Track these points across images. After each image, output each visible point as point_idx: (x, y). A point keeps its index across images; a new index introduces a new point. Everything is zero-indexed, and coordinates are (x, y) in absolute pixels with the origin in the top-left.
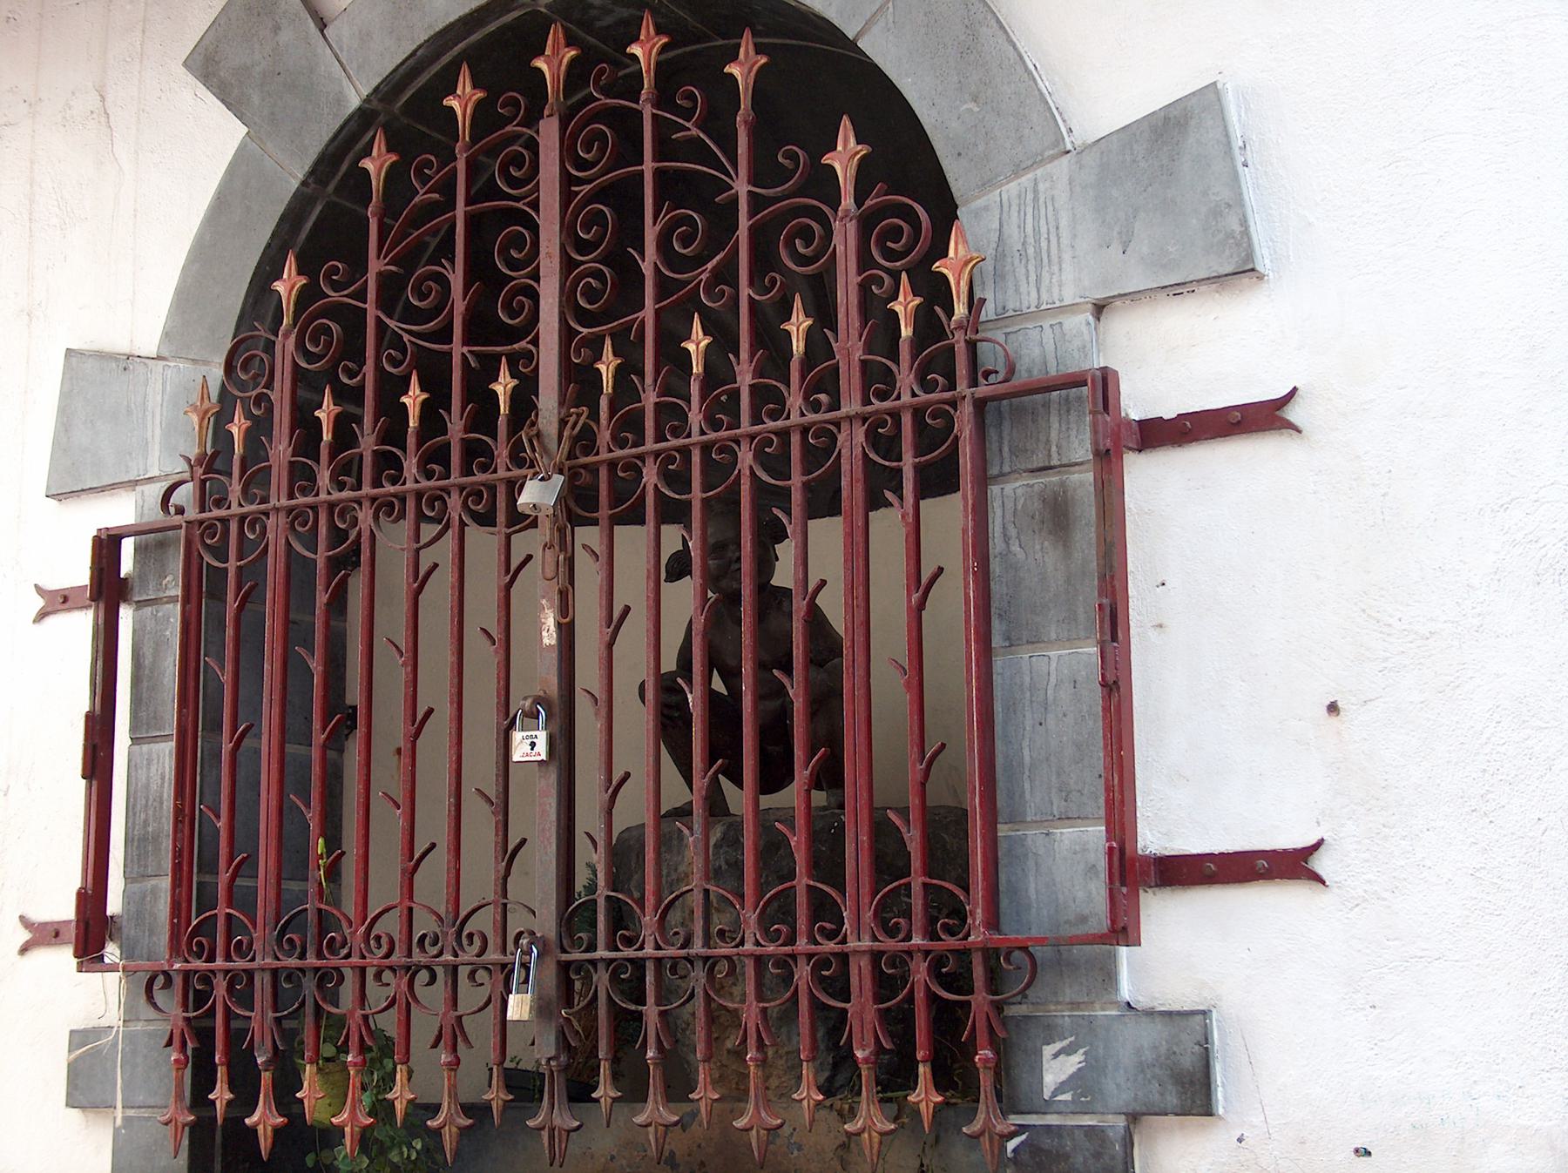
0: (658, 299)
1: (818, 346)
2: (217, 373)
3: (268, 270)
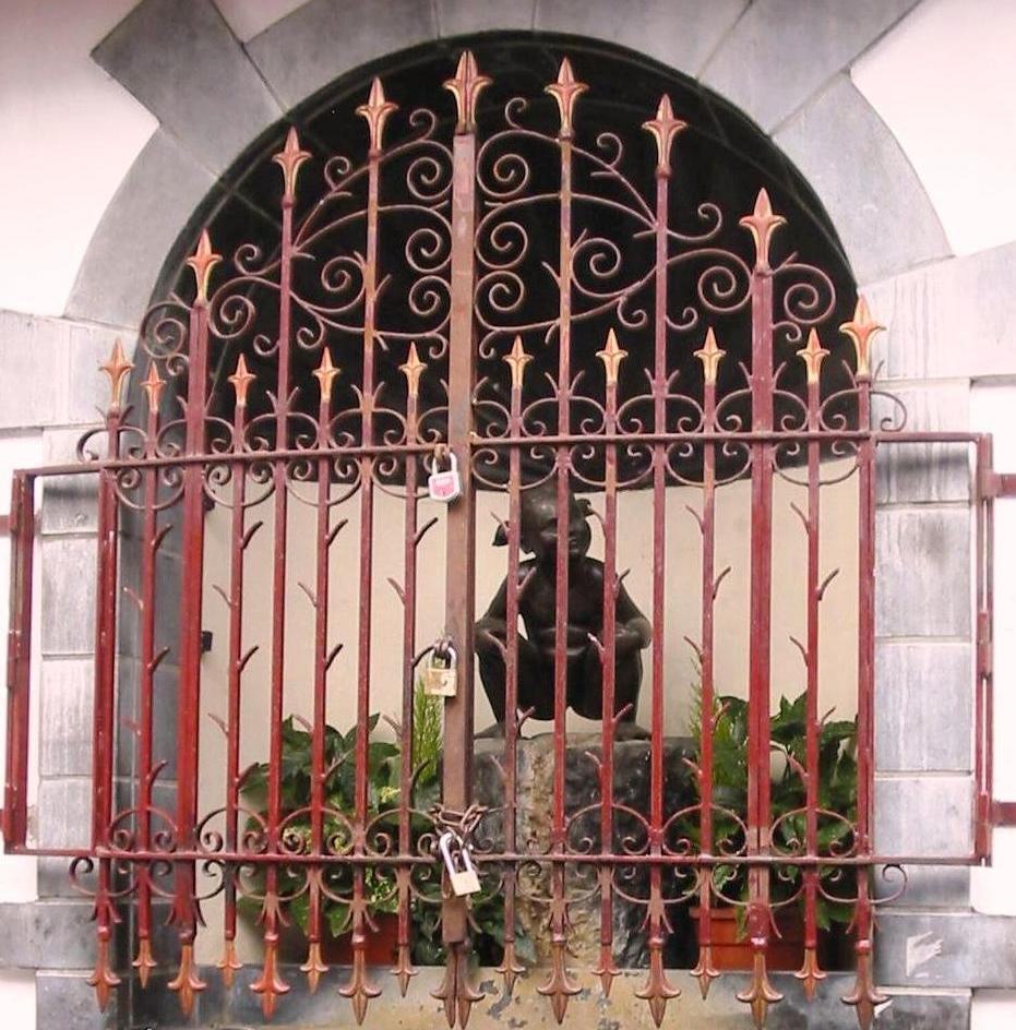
1: (731, 376)
2: (130, 338)
3: (185, 244)
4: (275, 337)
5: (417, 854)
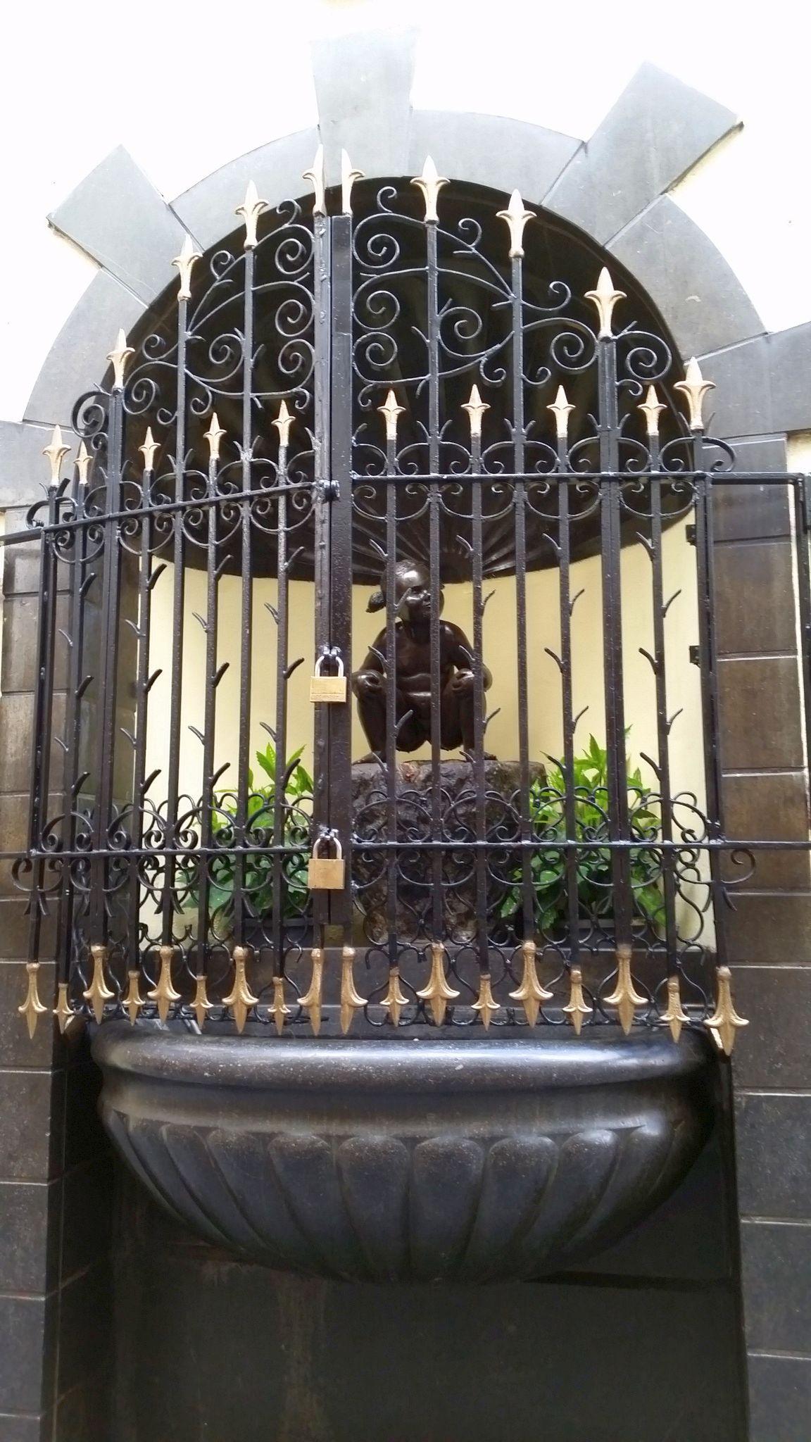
0: (241, 302)
4: (174, 408)
5: (215, 847)
